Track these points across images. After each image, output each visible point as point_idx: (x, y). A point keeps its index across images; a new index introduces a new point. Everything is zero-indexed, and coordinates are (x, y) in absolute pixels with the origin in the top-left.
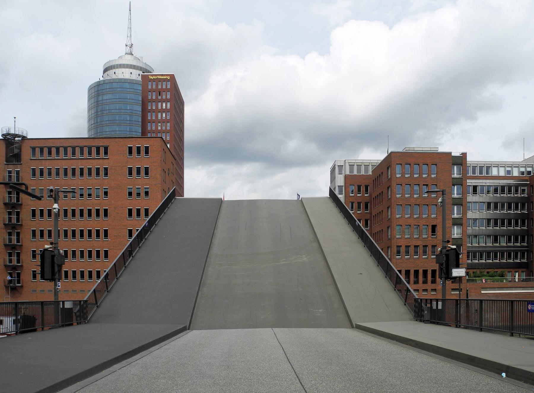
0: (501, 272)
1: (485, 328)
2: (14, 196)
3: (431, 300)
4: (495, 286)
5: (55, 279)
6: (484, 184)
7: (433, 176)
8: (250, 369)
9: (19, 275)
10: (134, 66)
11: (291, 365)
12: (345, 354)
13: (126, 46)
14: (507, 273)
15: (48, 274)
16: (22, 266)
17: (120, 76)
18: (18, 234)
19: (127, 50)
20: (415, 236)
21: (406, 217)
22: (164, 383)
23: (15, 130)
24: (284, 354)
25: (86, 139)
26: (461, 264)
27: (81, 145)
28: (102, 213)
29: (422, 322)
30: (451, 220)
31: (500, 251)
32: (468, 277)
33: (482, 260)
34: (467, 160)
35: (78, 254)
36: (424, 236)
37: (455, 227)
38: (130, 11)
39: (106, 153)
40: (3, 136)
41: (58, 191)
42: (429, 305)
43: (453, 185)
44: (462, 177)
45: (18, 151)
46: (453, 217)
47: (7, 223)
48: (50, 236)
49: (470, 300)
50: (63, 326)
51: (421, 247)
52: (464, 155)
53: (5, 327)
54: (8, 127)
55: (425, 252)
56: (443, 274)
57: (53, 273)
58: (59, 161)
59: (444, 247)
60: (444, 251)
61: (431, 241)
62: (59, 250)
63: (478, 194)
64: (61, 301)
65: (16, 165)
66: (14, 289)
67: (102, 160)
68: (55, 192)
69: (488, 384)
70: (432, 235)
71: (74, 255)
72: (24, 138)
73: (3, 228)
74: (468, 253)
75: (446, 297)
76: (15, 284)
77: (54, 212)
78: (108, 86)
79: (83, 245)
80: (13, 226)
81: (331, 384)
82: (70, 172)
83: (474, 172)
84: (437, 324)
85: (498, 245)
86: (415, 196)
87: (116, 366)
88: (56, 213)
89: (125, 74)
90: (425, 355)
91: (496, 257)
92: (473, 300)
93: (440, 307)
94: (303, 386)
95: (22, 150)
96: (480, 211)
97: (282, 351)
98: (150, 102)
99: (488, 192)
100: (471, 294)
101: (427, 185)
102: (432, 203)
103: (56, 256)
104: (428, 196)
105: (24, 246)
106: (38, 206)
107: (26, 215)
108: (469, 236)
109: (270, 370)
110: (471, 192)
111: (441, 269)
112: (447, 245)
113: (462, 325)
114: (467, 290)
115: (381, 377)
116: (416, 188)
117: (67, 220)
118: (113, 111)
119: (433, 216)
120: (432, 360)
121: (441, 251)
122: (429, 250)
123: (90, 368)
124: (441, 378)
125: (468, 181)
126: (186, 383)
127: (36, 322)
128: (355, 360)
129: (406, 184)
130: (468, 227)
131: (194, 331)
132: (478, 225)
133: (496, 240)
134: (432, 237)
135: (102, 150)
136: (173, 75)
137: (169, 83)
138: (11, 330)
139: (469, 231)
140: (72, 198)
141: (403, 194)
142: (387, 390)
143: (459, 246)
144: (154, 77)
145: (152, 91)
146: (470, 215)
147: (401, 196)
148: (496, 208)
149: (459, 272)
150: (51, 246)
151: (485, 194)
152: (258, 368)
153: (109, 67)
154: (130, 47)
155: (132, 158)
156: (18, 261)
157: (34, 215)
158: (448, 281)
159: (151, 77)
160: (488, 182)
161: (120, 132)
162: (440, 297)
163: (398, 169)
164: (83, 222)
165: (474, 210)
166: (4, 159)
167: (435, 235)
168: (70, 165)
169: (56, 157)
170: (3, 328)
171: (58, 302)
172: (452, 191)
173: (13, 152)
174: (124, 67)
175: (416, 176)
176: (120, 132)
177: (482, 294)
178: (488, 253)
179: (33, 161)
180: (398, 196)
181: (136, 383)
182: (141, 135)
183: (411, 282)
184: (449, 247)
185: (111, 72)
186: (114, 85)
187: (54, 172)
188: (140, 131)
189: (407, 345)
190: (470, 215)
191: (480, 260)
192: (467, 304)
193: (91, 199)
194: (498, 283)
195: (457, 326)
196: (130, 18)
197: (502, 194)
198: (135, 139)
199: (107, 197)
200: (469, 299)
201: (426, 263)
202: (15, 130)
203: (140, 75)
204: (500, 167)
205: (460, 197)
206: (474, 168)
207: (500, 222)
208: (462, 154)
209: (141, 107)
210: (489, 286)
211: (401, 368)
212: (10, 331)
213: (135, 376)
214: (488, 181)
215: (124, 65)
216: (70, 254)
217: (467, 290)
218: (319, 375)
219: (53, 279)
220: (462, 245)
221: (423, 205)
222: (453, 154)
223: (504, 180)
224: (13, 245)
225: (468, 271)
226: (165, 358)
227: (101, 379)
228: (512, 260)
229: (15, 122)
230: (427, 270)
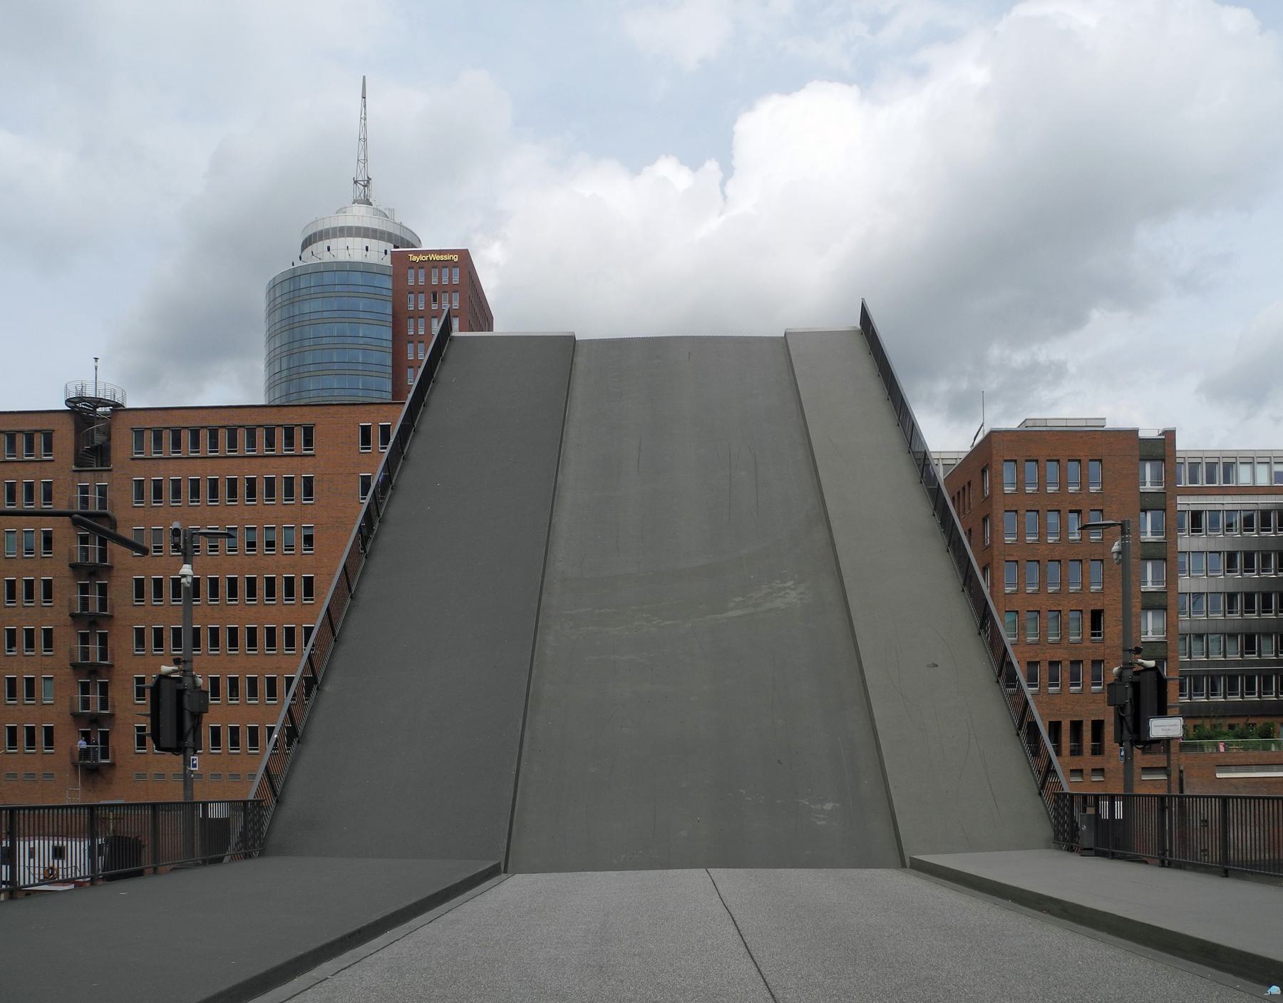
0: (1264, 724)
2: (94, 547)
3: (1097, 797)
4: (1252, 761)
5: (186, 748)
7: (1093, 489)
8: (654, 974)
10: (375, 231)
11: (756, 963)
12: (887, 934)
13: (356, 182)
15: (168, 737)
16: (112, 715)
17: (342, 257)
18: (104, 639)
19: (358, 194)
20: (1051, 639)
21: (1028, 592)
23: (96, 389)
24: (737, 936)
25: (260, 409)
27: (250, 422)
28: (299, 587)
29: (1074, 851)
31: (1260, 673)
34: (1177, 449)
35: (243, 687)
36: (1072, 638)
37: (1150, 614)
38: (364, 98)
39: (308, 442)
40: (68, 403)
41: (193, 534)
42: (1091, 811)
43: (1142, 511)
44: (1164, 489)
45: (105, 438)
46: (1142, 590)
48: (177, 643)
50: (204, 863)
51: (1066, 663)
52: (1169, 435)
53: (69, 865)
55: (1075, 679)
56: (1125, 732)
57: (181, 735)
59: (1127, 665)
60: (1128, 673)
62: (194, 677)
63: (1204, 532)
64: (199, 803)
65: (100, 473)
67: (300, 458)
68: (185, 536)
71: (235, 689)
72: (117, 407)
76: (96, 759)
77: (184, 583)
78: (312, 279)
79: (255, 666)
82: (223, 489)
83: (1193, 479)
85: (1254, 657)
86: (1051, 539)
87: (327, 967)
89: (351, 251)
91: (1250, 689)
92: (1196, 797)
93: (1119, 814)
95: (112, 438)
96: (1209, 574)
97: (732, 929)
98: (412, 318)
99: (1230, 526)
101: (1079, 512)
102: (1091, 555)
103: (188, 693)
104: (1081, 540)
105: (116, 667)
106: (148, 568)
107: (121, 593)
108: (1183, 637)
109: (704, 978)
110: (1186, 527)
111: (1120, 720)
112: (1136, 659)
114: (1181, 772)
115: (980, 995)
116: (1053, 519)
117: (218, 605)
118: (325, 340)
119: (1094, 588)
120: (1108, 953)
121: (1120, 675)
122: (1086, 671)
123: (262, 970)
125: (1180, 500)
127: (143, 856)
129: (1027, 511)
131: (517, 876)
132: (1205, 609)
133: (1249, 645)
134: (1092, 640)
135: (299, 436)
136: (466, 251)
137: (456, 271)
138: (85, 874)
139: (1184, 623)
140: (229, 551)
141: (1021, 535)
143: (1161, 660)
144: (421, 258)
145: (416, 290)
146: (1186, 584)
147: (1017, 540)
148: (1249, 565)
149: (1167, 728)
151: (1221, 531)
153: (315, 234)
154: (364, 186)
155: (370, 453)
156: (104, 705)
157: (140, 593)
159: (415, 258)
160: (1229, 502)
161: (342, 392)
162: (1119, 790)
163: (1008, 472)
164: (254, 609)
166: (71, 458)
167: (1100, 635)
168: (223, 471)
169: (192, 452)
171: (194, 805)
172: (1139, 525)
174: (350, 235)
175: (1051, 490)
176: (342, 392)
178: (1230, 677)
179: (138, 461)
180: (1009, 540)
182: (391, 398)
183: (1085, 750)
184: (1141, 664)
185: (319, 247)
186: (327, 278)
188: (389, 388)
189: (1041, 911)
190: (1186, 584)
192: (1182, 805)
193: (274, 554)
194: (1256, 752)
195: (1163, 862)
196: (363, 116)
197: (1263, 530)
198: (376, 407)
199: (312, 550)
200: (1185, 794)
202: (96, 389)
203: (389, 252)
204: (1258, 463)
206: (1194, 467)
207: (1259, 599)
208: (1165, 432)
209: (390, 331)
210: (1234, 761)
211: (1031, 971)
212: (82, 874)
213: (373, 991)
214: (1228, 499)
215: (350, 228)
216: (224, 686)
217: (1181, 772)
218: (826, 991)
219: (179, 749)
220: (1166, 659)
221: (1070, 560)
222: (1142, 435)
224: (91, 665)
226: (448, 945)
227: (289, 999)
228: (1274, 695)
229: (96, 369)
230: (1082, 721)
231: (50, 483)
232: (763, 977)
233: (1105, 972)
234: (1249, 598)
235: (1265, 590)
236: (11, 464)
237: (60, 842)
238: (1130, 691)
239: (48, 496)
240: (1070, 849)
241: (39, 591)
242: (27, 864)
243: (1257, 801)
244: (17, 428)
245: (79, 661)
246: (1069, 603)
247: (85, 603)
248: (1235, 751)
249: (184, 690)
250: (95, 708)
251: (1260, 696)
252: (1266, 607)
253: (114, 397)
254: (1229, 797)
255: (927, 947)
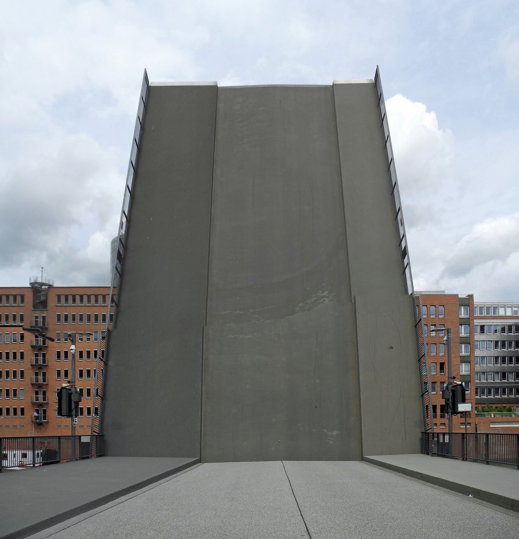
1: (497, 462)
3: (438, 434)
4: (504, 420)
5: (72, 415)
6: (491, 324)
9: (45, 412)
14: (515, 407)
15: (64, 411)
18: (44, 374)
22: (166, 515)
26: (467, 399)
27: (89, 293)
30: (459, 358)
31: (508, 387)
32: (477, 412)
33: (491, 395)
36: (432, 373)
37: (463, 364)
40: (31, 284)
42: (436, 439)
43: (460, 325)
47: (34, 364)
48: (66, 375)
49: (479, 434)
52: (471, 297)
53: (29, 460)
54: (35, 277)
56: (449, 409)
57: (70, 410)
58: (83, 308)
60: (450, 387)
61: (440, 378)
62: (76, 388)
63: (485, 333)
65: (43, 311)
66: (40, 424)
69: (492, 518)
70: (440, 373)
72: (50, 286)
73: (30, 369)
74: (476, 389)
75: (467, 432)
76: (41, 420)
80: (40, 367)
81: (332, 517)
82: (93, 318)
83: (481, 312)
84: (444, 457)
85: (506, 381)
87: (123, 498)
88: (73, 354)
90: (430, 488)
91: (504, 393)
92: (482, 434)
93: (447, 440)
94: (303, 518)
99: (496, 331)
100: (480, 428)
101: (435, 325)
102: (440, 341)
104: (436, 336)
107: (51, 357)
108: (477, 373)
110: (478, 331)
113: (469, 458)
114: (476, 425)
119: (441, 354)
124: (444, 510)
125: (475, 321)
126: (187, 515)
128: (360, 492)
130: (476, 364)
132: (486, 362)
133: (504, 376)
140: (94, 340)
142: (388, 523)
143: (467, 383)
146: (478, 353)
148: (503, 346)
150: (68, 385)
152: (262, 500)
156: (44, 399)
157: (59, 357)
158: (454, 415)
162: (447, 431)
165: (481, 348)
167: (443, 372)
170: (28, 461)
173: (40, 300)
177: (491, 428)
181: (138, 515)
184: (455, 383)
187: (78, 318)
189: (413, 477)
190: (478, 353)
191: (489, 395)
194: (506, 417)
195: (463, 459)
200: (478, 432)
201: (435, 399)
205: (467, 336)
206: (481, 308)
208: (468, 296)
210: (497, 421)
213: (139, 507)
214: (495, 321)
216: (85, 392)
217: (476, 425)
219: (69, 415)
220: (470, 382)
221: (432, 344)
222: (460, 296)
223: (512, 320)
224: (39, 384)
225: (477, 406)
228: (507, 395)
230: (436, 405)
231: (23, 314)
232: (297, 502)
233: (434, 500)
234: (504, 359)
235: (503, 355)
236: (7, 307)
237: (24, 452)
238: (451, 394)
239: (22, 319)
240: (428, 454)
241: (18, 356)
242: (13, 460)
243: (507, 435)
244: (10, 293)
245: (35, 383)
246: (431, 360)
247: (37, 361)
248: (498, 417)
249: (72, 393)
250: (41, 400)
251: (508, 396)
252: (511, 361)
253: (49, 282)
254: (489, 434)
255: (365, 491)
